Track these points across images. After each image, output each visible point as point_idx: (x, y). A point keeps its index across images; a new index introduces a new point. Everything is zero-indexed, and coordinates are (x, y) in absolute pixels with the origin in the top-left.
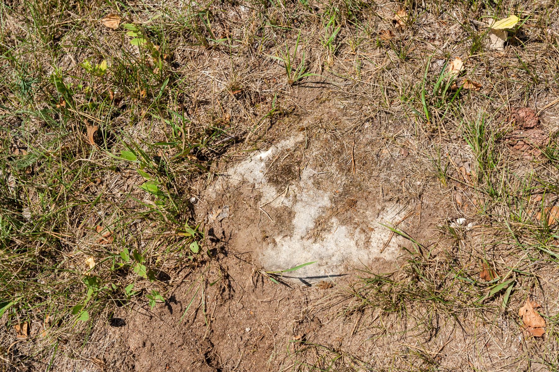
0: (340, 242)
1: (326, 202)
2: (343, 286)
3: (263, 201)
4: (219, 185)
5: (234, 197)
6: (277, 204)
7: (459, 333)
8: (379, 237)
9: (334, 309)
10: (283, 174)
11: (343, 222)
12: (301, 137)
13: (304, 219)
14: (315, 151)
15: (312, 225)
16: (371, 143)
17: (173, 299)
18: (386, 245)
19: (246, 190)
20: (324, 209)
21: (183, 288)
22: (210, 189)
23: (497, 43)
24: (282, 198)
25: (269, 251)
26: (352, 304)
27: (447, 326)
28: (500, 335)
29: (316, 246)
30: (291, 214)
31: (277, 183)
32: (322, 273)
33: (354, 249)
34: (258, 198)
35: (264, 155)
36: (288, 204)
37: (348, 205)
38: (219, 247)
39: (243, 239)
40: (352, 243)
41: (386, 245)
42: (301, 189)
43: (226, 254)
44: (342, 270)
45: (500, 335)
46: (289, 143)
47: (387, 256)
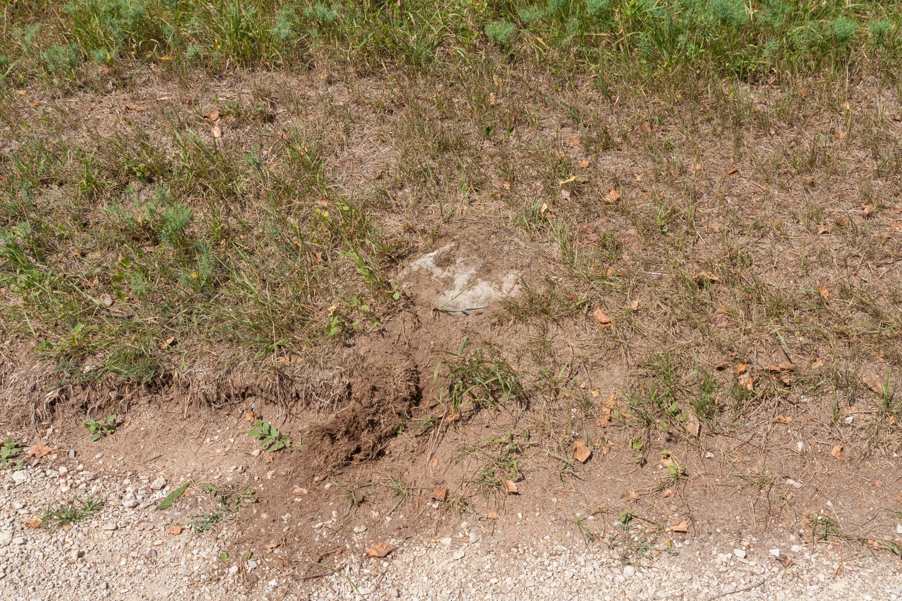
0: (484, 289)
1: (473, 271)
2: (487, 313)
3: (435, 275)
4: (405, 272)
5: (416, 276)
6: (443, 276)
7: (560, 331)
8: (507, 286)
9: (485, 324)
10: (444, 262)
11: (484, 280)
12: (453, 244)
13: (461, 280)
14: (463, 249)
15: (466, 283)
16: (496, 244)
17: (384, 330)
18: (512, 289)
19: (422, 272)
20: (472, 275)
21: (390, 324)
22: (400, 274)
23: (566, 194)
24: (446, 273)
25: (442, 298)
26: (495, 320)
27: (552, 328)
28: (585, 329)
29: (470, 293)
30: (452, 280)
31: (442, 266)
32: (475, 307)
33: (493, 292)
34: (431, 274)
35: (431, 254)
36: (450, 275)
37: (486, 271)
38: (410, 301)
39: (424, 295)
40: (491, 289)
41: (512, 289)
42: (457, 268)
43: (414, 305)
44: (486, 304)
45: (585, 329)
46: (447, 247)
47: (513, 294)
